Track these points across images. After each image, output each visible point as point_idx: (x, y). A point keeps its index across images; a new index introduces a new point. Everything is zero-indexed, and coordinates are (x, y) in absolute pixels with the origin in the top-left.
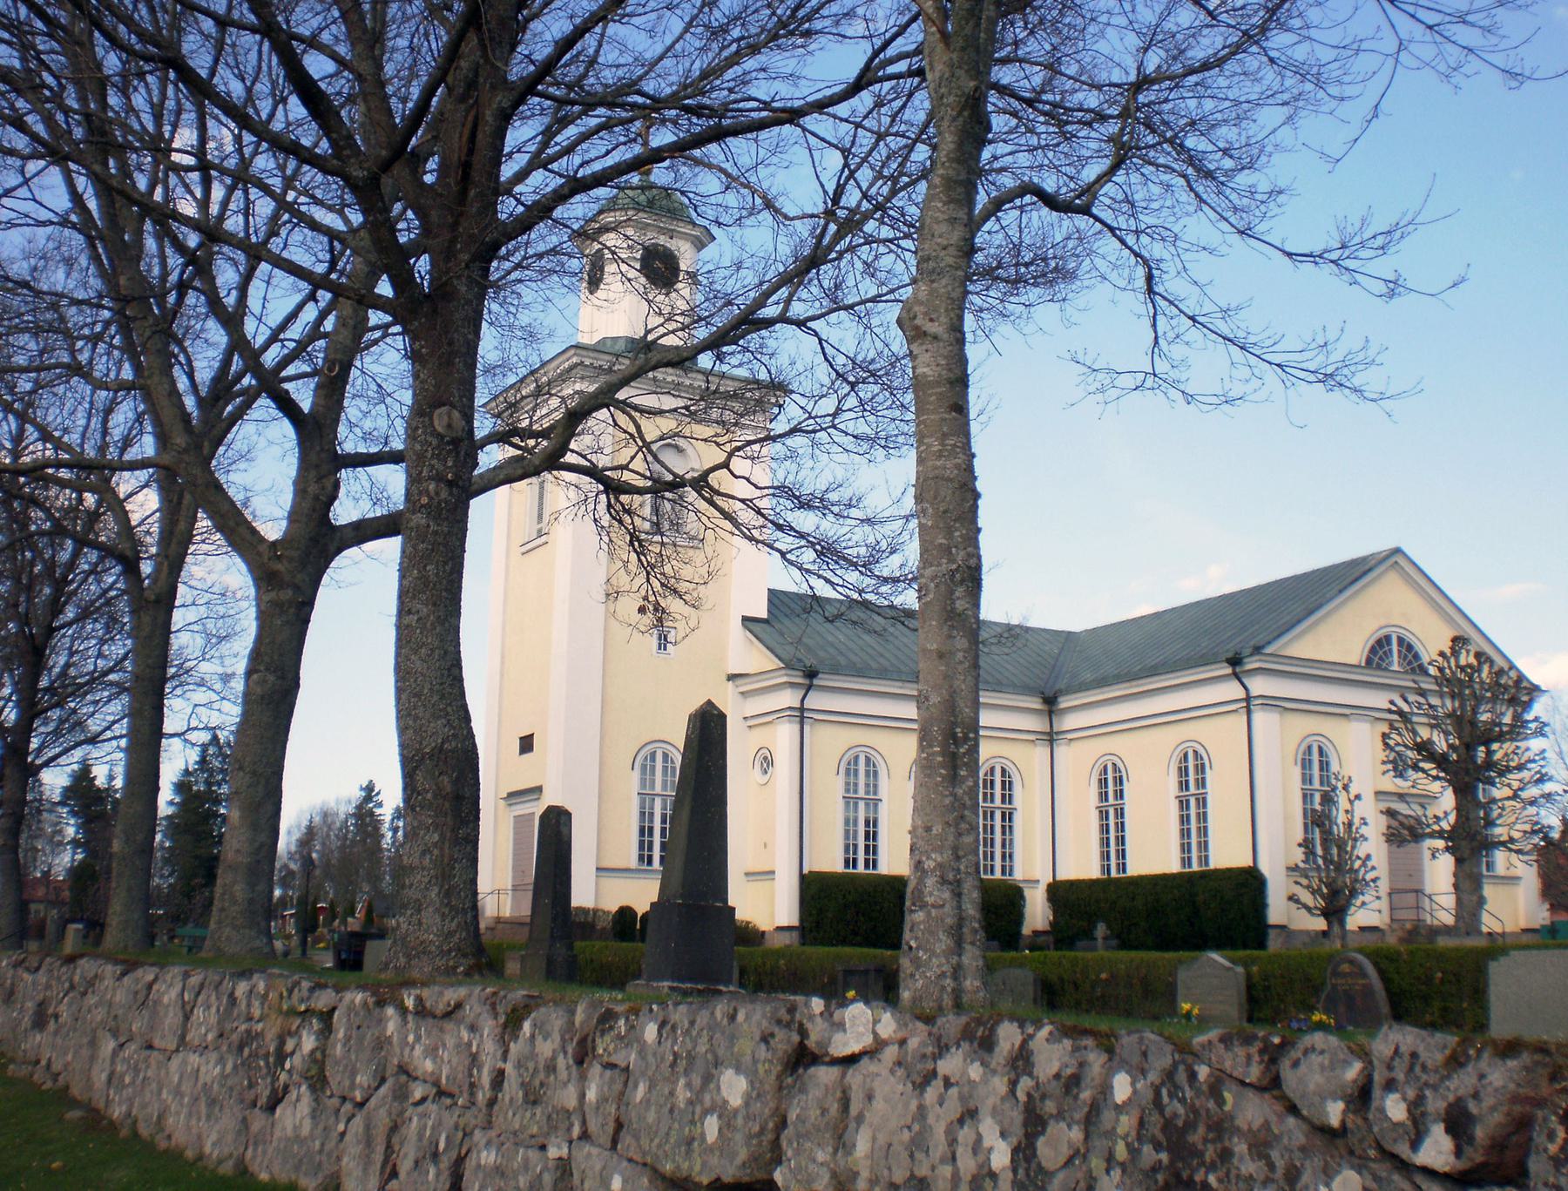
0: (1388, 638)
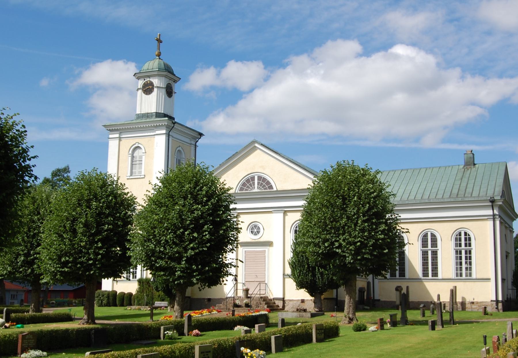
0: (253, 178)
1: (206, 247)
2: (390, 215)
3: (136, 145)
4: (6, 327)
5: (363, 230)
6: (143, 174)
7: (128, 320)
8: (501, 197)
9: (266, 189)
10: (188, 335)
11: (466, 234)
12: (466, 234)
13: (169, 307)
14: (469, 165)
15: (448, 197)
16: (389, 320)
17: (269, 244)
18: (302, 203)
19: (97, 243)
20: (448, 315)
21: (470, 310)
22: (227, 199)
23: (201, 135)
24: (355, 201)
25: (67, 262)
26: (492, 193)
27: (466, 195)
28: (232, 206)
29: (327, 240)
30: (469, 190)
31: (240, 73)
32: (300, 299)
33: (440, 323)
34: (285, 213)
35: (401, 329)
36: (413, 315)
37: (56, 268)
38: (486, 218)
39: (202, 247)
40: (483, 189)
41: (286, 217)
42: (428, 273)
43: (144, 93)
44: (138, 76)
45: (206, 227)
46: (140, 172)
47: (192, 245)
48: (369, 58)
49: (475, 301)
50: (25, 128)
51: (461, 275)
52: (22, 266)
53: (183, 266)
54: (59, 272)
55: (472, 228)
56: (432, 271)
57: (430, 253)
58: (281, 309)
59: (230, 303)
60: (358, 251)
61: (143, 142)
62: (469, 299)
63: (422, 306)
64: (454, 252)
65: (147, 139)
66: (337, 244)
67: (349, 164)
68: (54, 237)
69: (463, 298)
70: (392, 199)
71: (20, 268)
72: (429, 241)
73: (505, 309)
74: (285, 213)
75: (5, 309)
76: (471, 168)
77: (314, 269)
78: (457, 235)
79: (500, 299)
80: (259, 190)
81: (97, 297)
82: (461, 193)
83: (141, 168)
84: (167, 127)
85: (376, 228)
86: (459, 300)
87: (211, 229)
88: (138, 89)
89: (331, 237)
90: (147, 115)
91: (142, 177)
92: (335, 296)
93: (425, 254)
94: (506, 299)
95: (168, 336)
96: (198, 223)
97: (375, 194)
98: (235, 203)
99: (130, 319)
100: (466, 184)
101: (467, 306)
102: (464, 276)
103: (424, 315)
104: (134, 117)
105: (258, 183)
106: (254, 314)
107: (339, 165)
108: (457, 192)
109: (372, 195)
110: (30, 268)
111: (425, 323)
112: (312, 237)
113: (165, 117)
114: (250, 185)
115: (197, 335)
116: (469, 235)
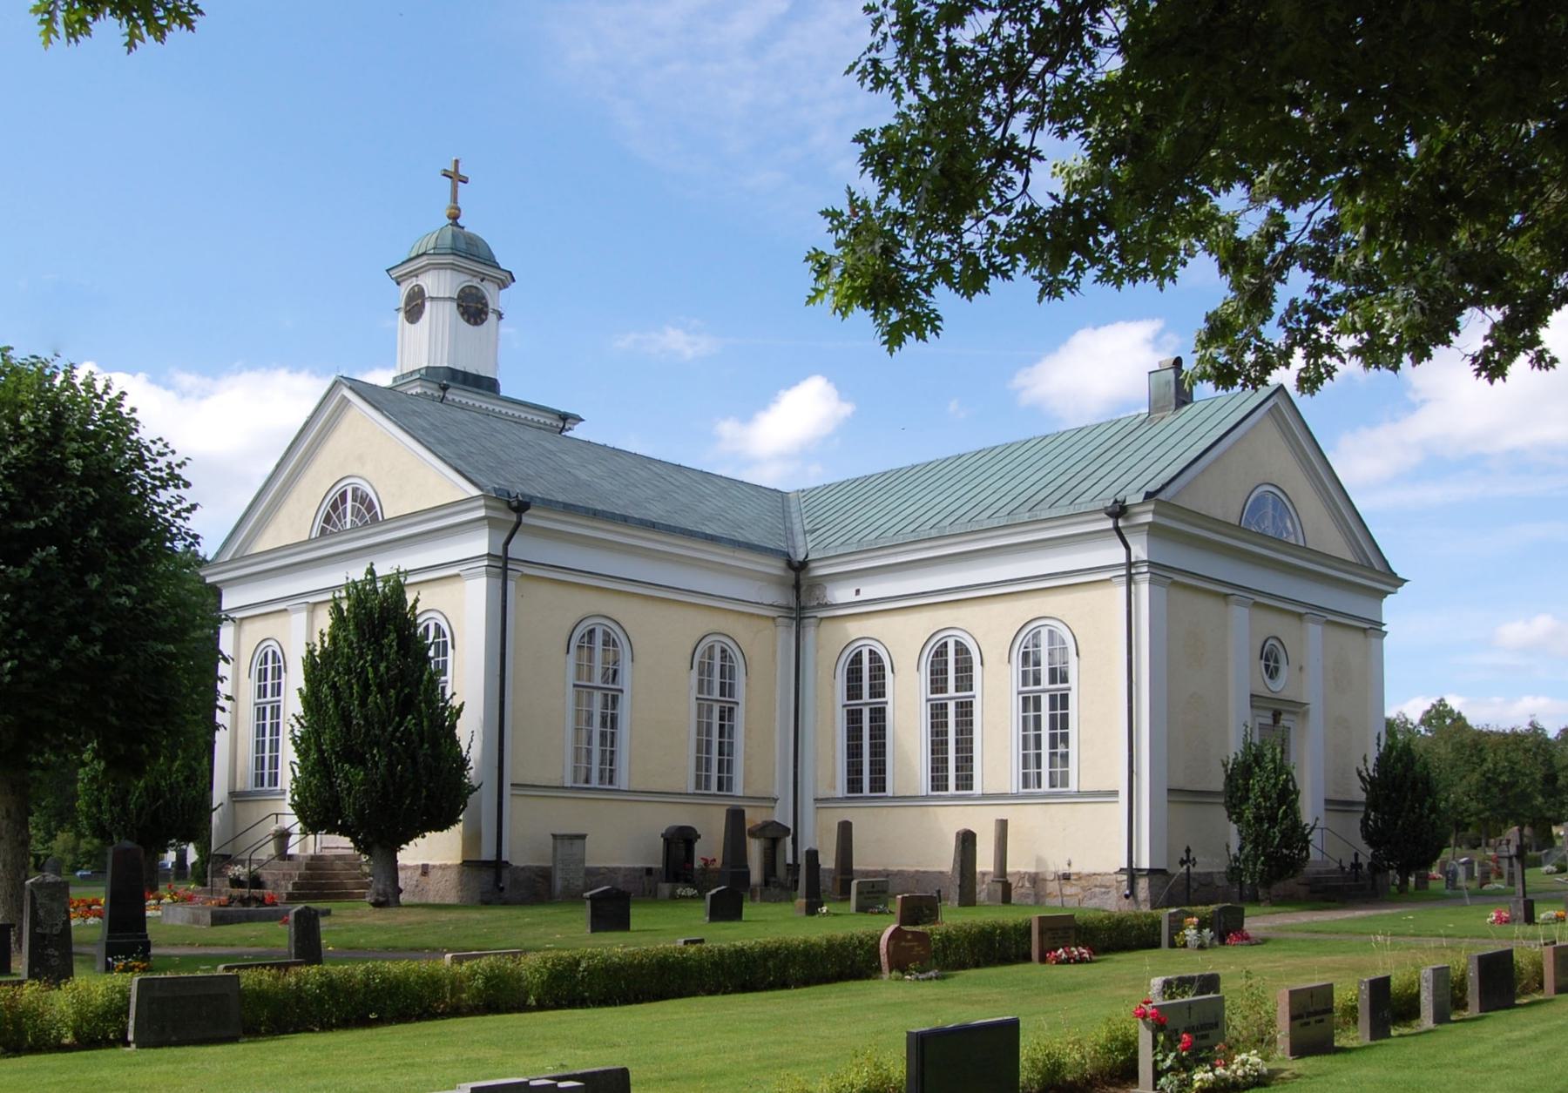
14: (1163, 409)
49: (1073, 869)
64: (1017, 703)
72: (950, 667)
102: (595, 783)
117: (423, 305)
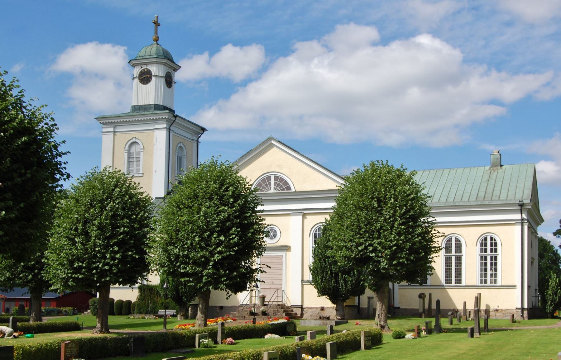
0: (269, 178)
1: (234, 251)
2: (425, 218)
3: (133, 140)
4: (15, 337)
5: (399, 234)
6: (141, 172)
7: (139, 329)
8: (531, 201)
9: (283, 189)
10: (222, 343)
11: (492, 239)
12: (492, 239)
13: (179, 316)
14: (496, 166)
15: (474, 200)
16: (425, 328)
17: (287, 248)
18: (332, 204)
19: (112, 246)
20: (481, 322)
21: (494, 318)
22: (254, 200)
23: (203, 130)
24: (391, 203)
25: (80, 268)
26: (521, 196)
27: (493, 198)
28: (259, 208)
29: (361, 244)
30: (497, 193)
31: (234, 60)
32: (320, 306)
33: (477, 330)
34: (304, 215)
35: (436, 338)
36: (445, 323)
37: (68, 273)
38: (514, 222)
39: (230, 251)
40: (511, 193)
41: (305, 220)
42: (451, 280)
43: (141, 82)
44: (133, 63)
45: (234, 229)
46: (138, 170)
47: (219, 249)
48: (387, 47)
49: (499, 308)
50: (54, 121)
51: (486, 282)
52: (22, 272)
53: (210, 271)
54: (71, 277)
55: (499, 233)
56: (455, 277)
57: (453, 259)
58: (299, 317)
59: (246, 311)
60: (393, 256)
61: (141, 137)
62: (493, 307)
63: (450, 313)
65: (146, 133)
66: (371, 249)
67: (383, 164)
68: (64, 241)
69: (487, 306)
70: (429, 203)
71: (20, 274)
72: (454, 246)
73: (530, 317)
74: (304, 215)
75: (11, 318)
76: (497, 169)
77: (337, 275)
78: (482, 240)
79: (526, 306)
80: (275, 191)
81: (92, 305)
82: (489, 195)
83: (138, 165)
84: (168, 120)
85: (413, 232)
86: (483, 307)
87: (238, 232)
88: (133, 79)
89: (365, 240)
90: (145, 108)
91: (139, 175)
92: (356, 304)
93: (448, 260)
94: (531, 307)
95: (204, 344)
96: (226, 227)
97: (412, 196)
98: (262, 205)
99: (141, 328)
100: (492, 187)
101: (491, 313)
103: (451, 324)
104: (129, 110)
105: (275, 184)
106: (276, 322)
107: (373, 164)
108: (483, 195)
109: (410, 197)
110: (31, 273)
111: (465, 331)
112: (344, 241)
113: (164, 110)
114: (266, 185)
115: (231, 343)
116: (495, 240)
117: (151, 78)
